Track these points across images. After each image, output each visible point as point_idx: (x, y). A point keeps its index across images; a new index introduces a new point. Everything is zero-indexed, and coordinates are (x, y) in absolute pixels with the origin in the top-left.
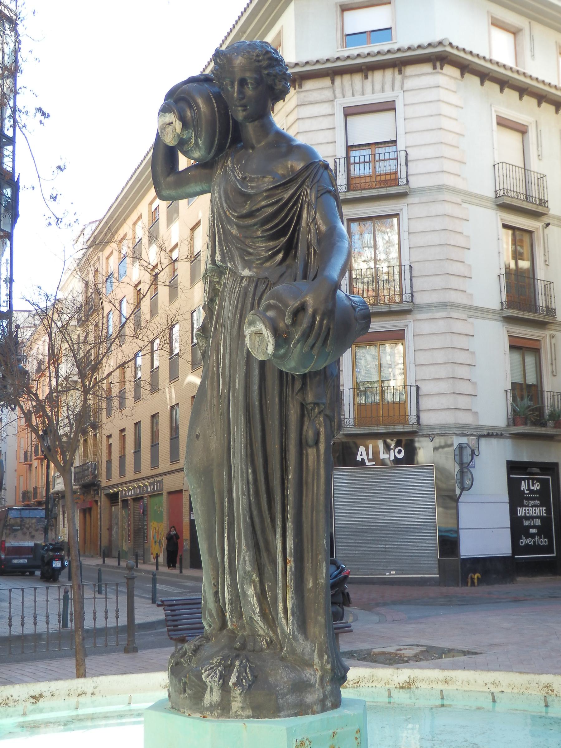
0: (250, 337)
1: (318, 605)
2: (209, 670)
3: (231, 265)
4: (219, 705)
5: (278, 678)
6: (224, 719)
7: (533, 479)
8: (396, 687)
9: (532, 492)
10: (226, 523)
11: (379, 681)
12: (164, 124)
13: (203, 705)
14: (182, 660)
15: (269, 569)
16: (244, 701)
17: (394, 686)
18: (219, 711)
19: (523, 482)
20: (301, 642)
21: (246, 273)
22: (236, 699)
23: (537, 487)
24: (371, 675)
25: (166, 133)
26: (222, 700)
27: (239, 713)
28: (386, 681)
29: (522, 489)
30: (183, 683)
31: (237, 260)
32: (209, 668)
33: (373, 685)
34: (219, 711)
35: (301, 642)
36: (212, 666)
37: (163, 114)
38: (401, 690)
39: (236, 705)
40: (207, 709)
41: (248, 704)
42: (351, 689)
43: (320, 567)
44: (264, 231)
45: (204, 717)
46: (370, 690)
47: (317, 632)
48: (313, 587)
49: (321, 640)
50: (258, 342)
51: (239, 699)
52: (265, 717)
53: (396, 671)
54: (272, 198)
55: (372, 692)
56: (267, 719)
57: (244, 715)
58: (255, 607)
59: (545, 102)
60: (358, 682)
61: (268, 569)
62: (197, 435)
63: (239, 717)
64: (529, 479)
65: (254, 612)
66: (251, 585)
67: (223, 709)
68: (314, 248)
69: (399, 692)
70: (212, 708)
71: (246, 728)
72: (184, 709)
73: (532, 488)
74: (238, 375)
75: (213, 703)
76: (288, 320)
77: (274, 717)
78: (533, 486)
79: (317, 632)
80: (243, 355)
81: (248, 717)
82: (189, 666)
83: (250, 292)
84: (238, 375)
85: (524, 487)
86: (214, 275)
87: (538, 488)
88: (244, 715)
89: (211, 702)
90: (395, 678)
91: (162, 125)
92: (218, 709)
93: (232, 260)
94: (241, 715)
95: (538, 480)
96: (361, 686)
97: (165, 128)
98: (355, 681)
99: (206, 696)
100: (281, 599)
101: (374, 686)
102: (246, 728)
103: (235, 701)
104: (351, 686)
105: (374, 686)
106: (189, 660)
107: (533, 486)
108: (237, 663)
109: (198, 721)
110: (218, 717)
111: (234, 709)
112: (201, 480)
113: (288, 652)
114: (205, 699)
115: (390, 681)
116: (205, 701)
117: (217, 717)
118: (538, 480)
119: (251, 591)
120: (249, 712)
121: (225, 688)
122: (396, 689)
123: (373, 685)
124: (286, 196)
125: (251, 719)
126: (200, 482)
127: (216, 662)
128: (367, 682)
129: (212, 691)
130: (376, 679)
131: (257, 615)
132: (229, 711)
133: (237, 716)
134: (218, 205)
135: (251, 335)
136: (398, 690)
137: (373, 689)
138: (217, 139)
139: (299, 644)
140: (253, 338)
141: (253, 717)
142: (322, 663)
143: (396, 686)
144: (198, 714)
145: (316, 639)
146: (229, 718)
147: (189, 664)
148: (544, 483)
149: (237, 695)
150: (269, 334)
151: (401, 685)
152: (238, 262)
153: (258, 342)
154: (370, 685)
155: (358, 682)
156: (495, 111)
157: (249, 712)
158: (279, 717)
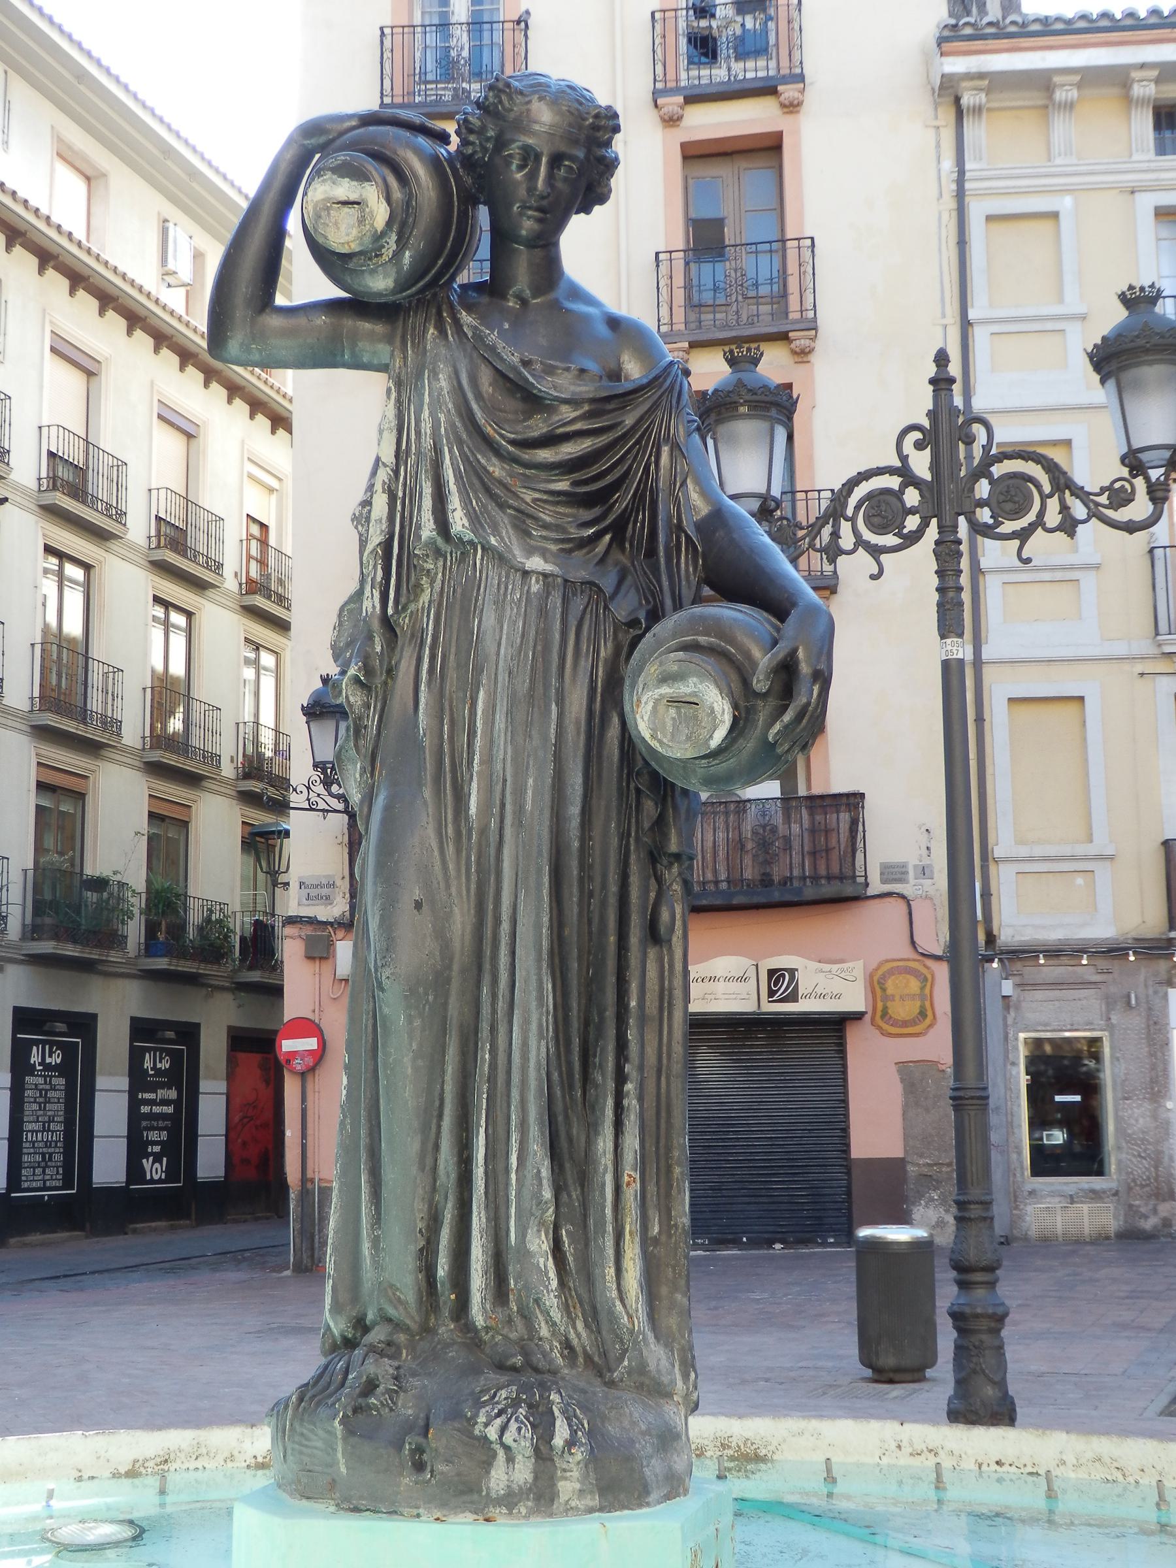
0: (655, 708)
1: (674, 1270)
2: (499, 1415)
3: (496, 541)
4: (530, 1489)
5: (626, 1424)
6: (539, 1519)
7: (52, 1044)
8: (248, 1467)
9: (159, 1072)
10: (485, 1096)
11: (212, 1455)
12: (327, 199)
13: (488, 1494)
14: (373, 1400)
15: (574, 1197)
16: (584, 1478)
17: (245, 1465)
18: (530, 1504)
19: (35, 1048)
20: (652, 1346)
21: (536, 563)
22: (568, 1474)
23: (56, 1059)
24: (196, 1442)
25: (333, 220)
26: (536, 1478)
27: (573, 1504)
28: (227, 1454)
29: (32, 1062)
30: (410, 1449)
31: (507, 532)
32: (496, 1411)
33: (199, 1464)
34: (530, 1504)
35: (652, 1346)
36: (500, 1407)
37: (335, 177)
38: (260, 1472)
39: (567, 1487)
40: (499, 1502)
41: (592, 1484)
42: (149, 1477)
43: (679, 1192)
44: (575, 483)
45: (487, 1520)
46: (192, 1475)
47: (674, 1327)
48: (660, 1232)
49: (683, 1342)
50: (674, 719)
51: (576, 1474)
52: (623, 1507)
53: (249, 1430)
54: (598, 420)
55: (196, 1481)
56: (626, 1512)
57: (582, 1507)
58: (548, 1279)
59: (56, 268)
60: (166, 1461)
61: (570, 1196)
62: (416, 901)
63: (570, 1513)
64: (44, 1042)
65: (547, 1287)
66: (539, 1231)
67: (538, 1498)
68: (687, 536)
69: (255, 1476)
70: (510, 1500)
71: (606, 1532)
72: (418, 1508)
73: (48, 1060)
74: (531, 781)
75: (515, 1486)
76: (763, 683)
77: (640, 1506)
78: (50, 1056)
79: (674, 1327)
80: (545, 738)
81: (591, 1510)
82: (393, 1413)
83: (555, 608)
84: (531, 781)
85: (36, 1059)
86: (427, 556)
87: (59, 1061)
88: (582, 1507)
89: (508, 1487)
90: (247, 1445)
91: (323, 200)
92: (528, 1499)
93: (496, 531)
94: (577, 1508)
95: (61, 1045)
96: (172, 1469)
97: (328, 209)
98: (158, 1460)
99: (493, 1473)
100: (612, 1259)
101: (201, 1467)
102: (606, 1532)
103: (566, 1479)
104: (149, 1470)
105: (201, 1467)
106: (392, 1400)
107: (50, 1056)
108: (555, 1397)
109: (469, 1528)
110: (526, 1517)
111: (563, 1498)
112: (427, 1001)
113: (630, 1373)
114: (493, 1480)
115: (236, 1453)
116: (492, 1484)
117: (525, 1517)
118: (61, 1045)
119: (539, 1244)
120: (595, 1501)
121: (543, 1455)
122: (248, 1471)
123: (199, 1464)
124: (629, 421)
125: (597, 1514)
126: (424, 1005)
127: (505, 1399)
128: (185, 1461)
129: (510, 1460)
130: (204, 1451)
131: (552, 1295)
132: (552, 1501)
133: (569, 1510)
134: (447, 407)
135: (657, 702)
136: (253, 1472)
137: (199, 1475)
138: (440, 262)
139: (651, 1351)
140: (661, 708)
141: (601, 1509)
142: (688, 1389)
143: (248, 1463)
144: (468, 1514)
145: (672, 1342)
146: (551, 1515)
147: (391, 1410)
148: (69, 1051)
149: (572, 1465)
150: (726, 708)
151: (260, 1460)
152: (509, 538)
153: (674, 719)
154: (192, 1465)
155: (166, 1461)
156: (51, 322)
157: (593, 1499)
158: (648, 1504)
